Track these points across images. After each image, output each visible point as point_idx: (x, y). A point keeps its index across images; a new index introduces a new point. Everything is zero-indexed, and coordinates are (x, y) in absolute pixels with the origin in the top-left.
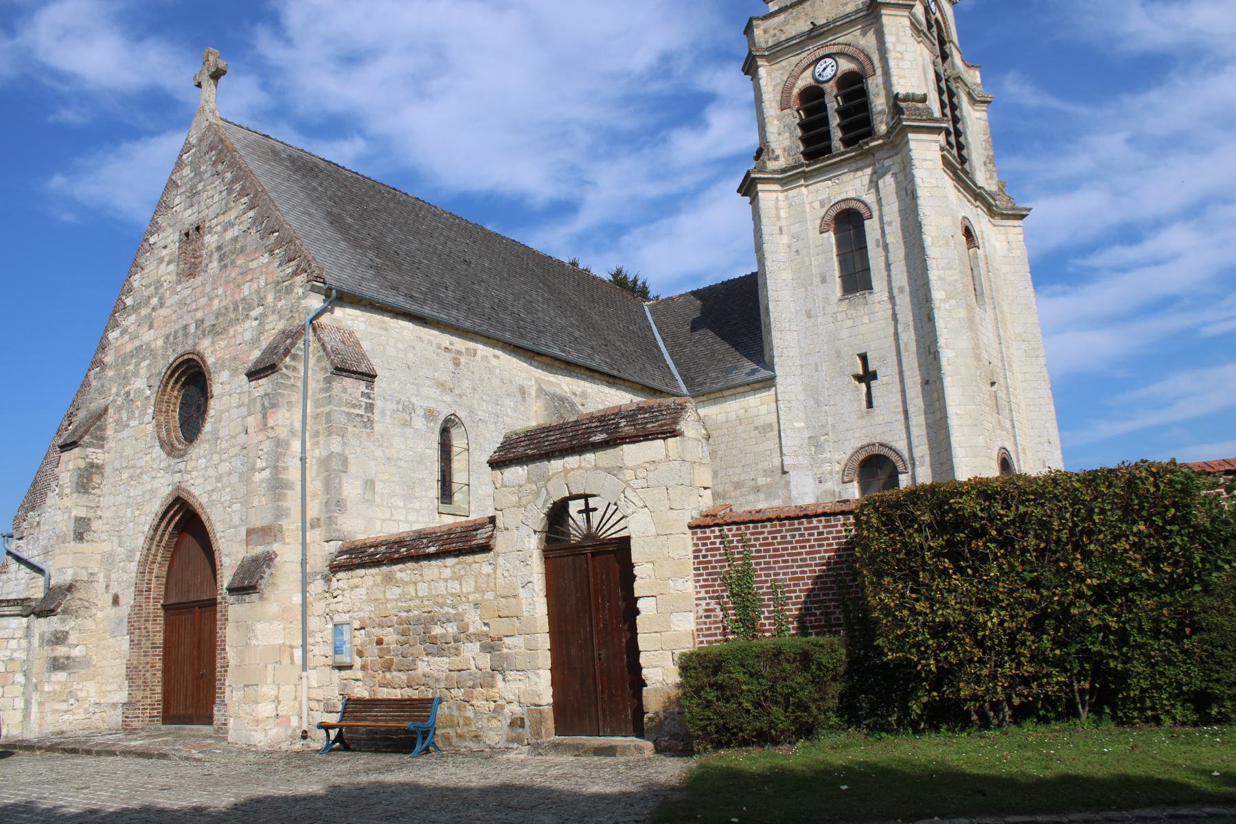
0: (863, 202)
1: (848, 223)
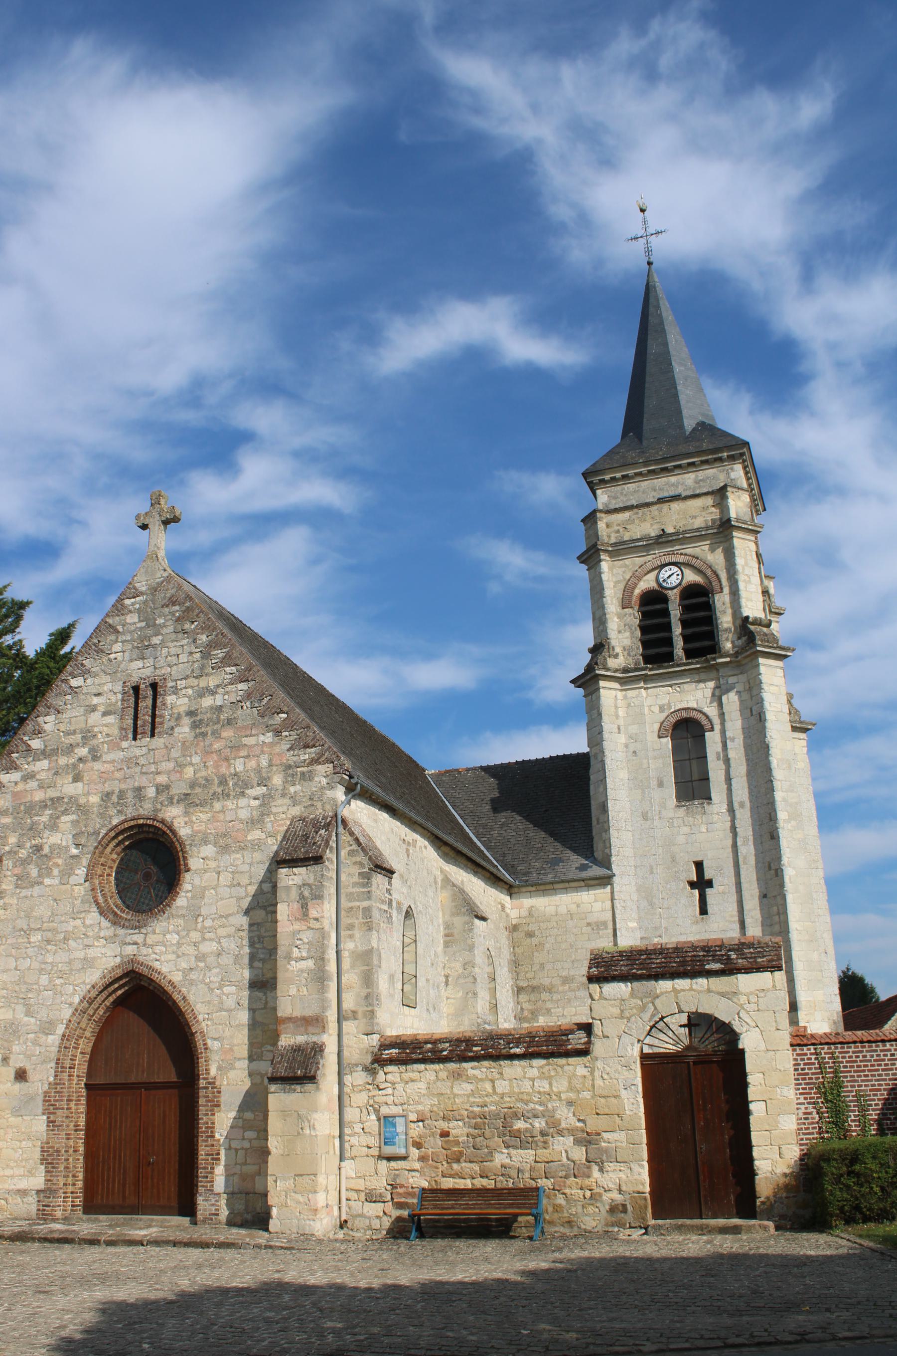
0: (704, 714)
1: (687, 731)
